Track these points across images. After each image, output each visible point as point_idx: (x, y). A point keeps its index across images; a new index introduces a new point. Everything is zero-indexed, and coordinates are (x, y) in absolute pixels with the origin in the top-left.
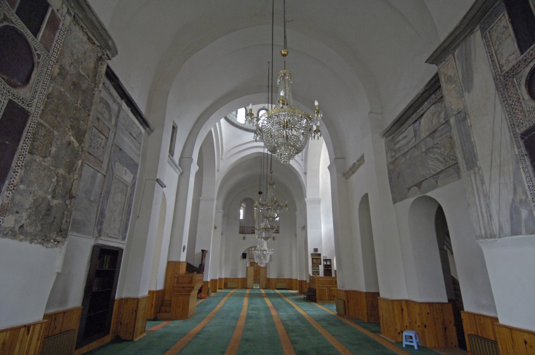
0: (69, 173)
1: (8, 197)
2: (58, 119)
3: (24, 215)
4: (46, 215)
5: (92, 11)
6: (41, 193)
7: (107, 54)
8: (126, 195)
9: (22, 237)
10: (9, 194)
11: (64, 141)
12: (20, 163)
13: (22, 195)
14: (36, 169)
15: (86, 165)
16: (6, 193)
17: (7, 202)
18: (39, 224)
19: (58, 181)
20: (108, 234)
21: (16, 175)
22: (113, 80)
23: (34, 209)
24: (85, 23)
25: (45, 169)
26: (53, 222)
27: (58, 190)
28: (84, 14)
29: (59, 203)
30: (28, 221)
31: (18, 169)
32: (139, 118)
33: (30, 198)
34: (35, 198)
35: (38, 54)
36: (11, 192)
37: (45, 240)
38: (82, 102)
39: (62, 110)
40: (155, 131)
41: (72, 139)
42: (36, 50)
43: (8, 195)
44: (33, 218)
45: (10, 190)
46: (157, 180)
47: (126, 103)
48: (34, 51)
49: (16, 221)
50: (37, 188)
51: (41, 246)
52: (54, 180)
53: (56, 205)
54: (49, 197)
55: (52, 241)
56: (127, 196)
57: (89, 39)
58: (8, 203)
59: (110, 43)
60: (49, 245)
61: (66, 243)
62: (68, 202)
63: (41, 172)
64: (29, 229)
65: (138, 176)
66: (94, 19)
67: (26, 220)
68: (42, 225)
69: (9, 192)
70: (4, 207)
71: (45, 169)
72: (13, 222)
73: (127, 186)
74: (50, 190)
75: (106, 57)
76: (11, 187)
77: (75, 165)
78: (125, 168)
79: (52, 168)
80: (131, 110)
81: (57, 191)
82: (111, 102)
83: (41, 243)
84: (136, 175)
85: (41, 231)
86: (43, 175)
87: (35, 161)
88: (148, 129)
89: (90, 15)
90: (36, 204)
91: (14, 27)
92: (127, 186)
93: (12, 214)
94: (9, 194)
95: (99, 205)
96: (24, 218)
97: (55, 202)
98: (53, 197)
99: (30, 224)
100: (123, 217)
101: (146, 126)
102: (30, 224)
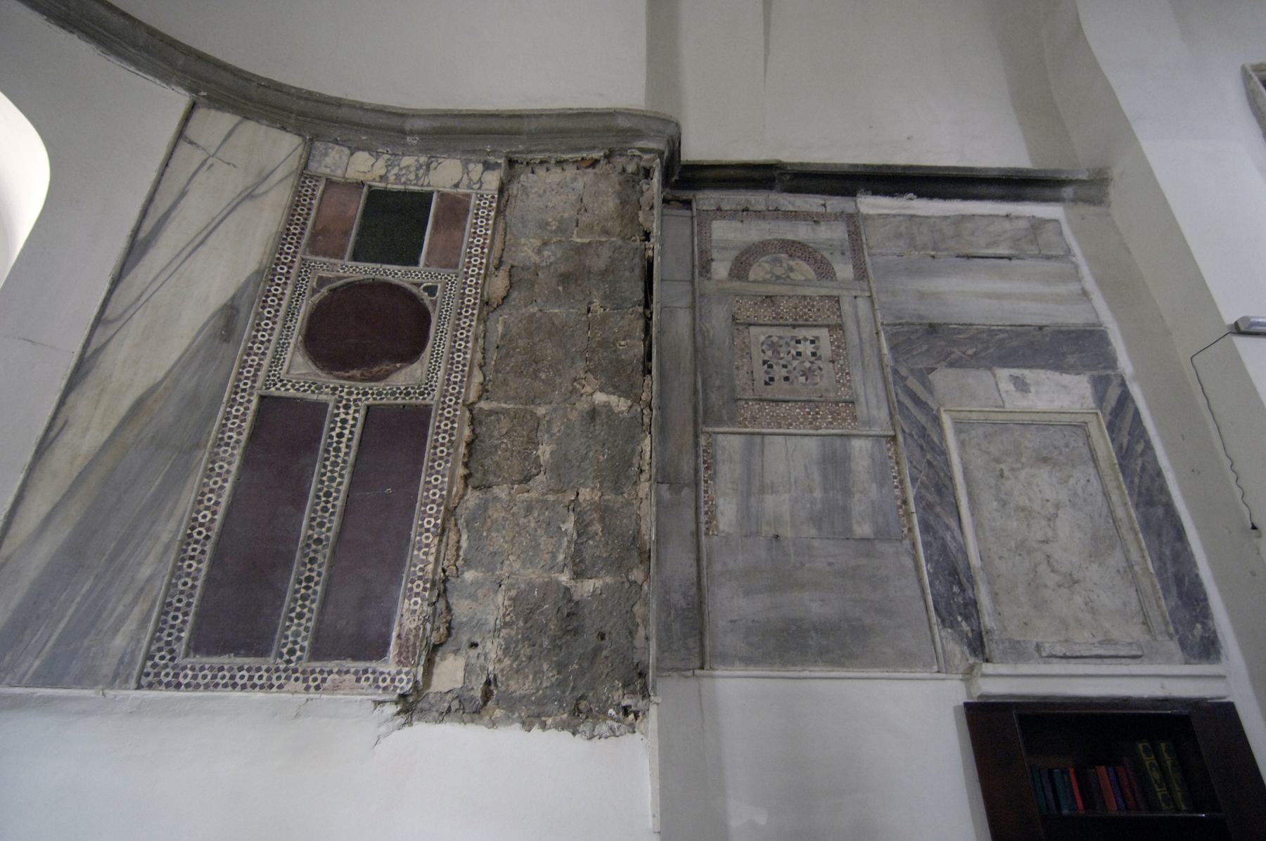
0: (617, 489)
1: (414, 612)
2: (543, 376)
3: (492, 648)
4: (566, 632)
5: (528, 116)
6: (534, 575)
7: (641, 150)
8: (1094, 460)
9: (498, 713)
10: (416, 603)
11: (574, 416)
12: (429, 522)
13: (473, 597)
14: (505, 519)
15: (720, 437)
16: (406, 606)
17: (413, 626)
18: (545, 667)
19: (582, 528)
20: (1038, 647)
21: (426, 554)
22: (772, 180)
23: (521, 623)
24: (541, 147)
25: (529, 510)
26: (597, 651)
27: (592, 549)
28: (524, 137)
29: (606, 587)
30: (507, 662)
31: (427, 538)
32: (983, 189)
33: (500, 599)
34: (513, 593)
35: (426, 289)
36: (419, 600)
37: (579, 713)
38: (605, 297)
39: (549, 351)
40: (1115, 173)
41: (600, 398)
42: (418, 285)
43: (412, 607)
44: (525, 651)
45: (417, 594)
46: (1238, 330)
47: (875, 193)
48: (414, 290)
49: (468, 669)
50: (517, 566)
51: (567, 734)
52: (569, 526)
53: (593, 594)
54: (564, 578)
55: (611, 711)
56: (1103, 464)
57: (580, 164)
58: (417, 628)
59: (622, 123)
60: (603, 728)
61: (653, 710)
62: (637, 575)
63: (522, 521)
64: (520, 687)
65: (1125, 364)
66: (545, 123)
67: (500, 661)
68: (561, 667)
69: (414, 599)
70: (408, 640)
71: (529, 510)
72: (460, 674)
73: (1083, 426)
74: (561, 557)
75: (646, 157)
76: (418, 586)
77: (636, 460)
78: (1004, 373)
79: (551, 498)
80: (920, 195)
81: (587, 554)
82: (802, 232)
83: (562, 726)
84: (1111, 362)
85: (561, 684)
86: (533, 524)
87: (496, 499)
88: (1068, 192)
89: (534, 125)
90: (525, 608)
91: (348, 284)
92: (1083, 426)
93: (456, 652)
94: (416, 603)
95: (914, 545)
96: (493, 656)
97: (588, 586)
98: (578, 575)
99: (517, 671)
100: (1135, 556)
101: (1048, 192)
102: (517, 671)
